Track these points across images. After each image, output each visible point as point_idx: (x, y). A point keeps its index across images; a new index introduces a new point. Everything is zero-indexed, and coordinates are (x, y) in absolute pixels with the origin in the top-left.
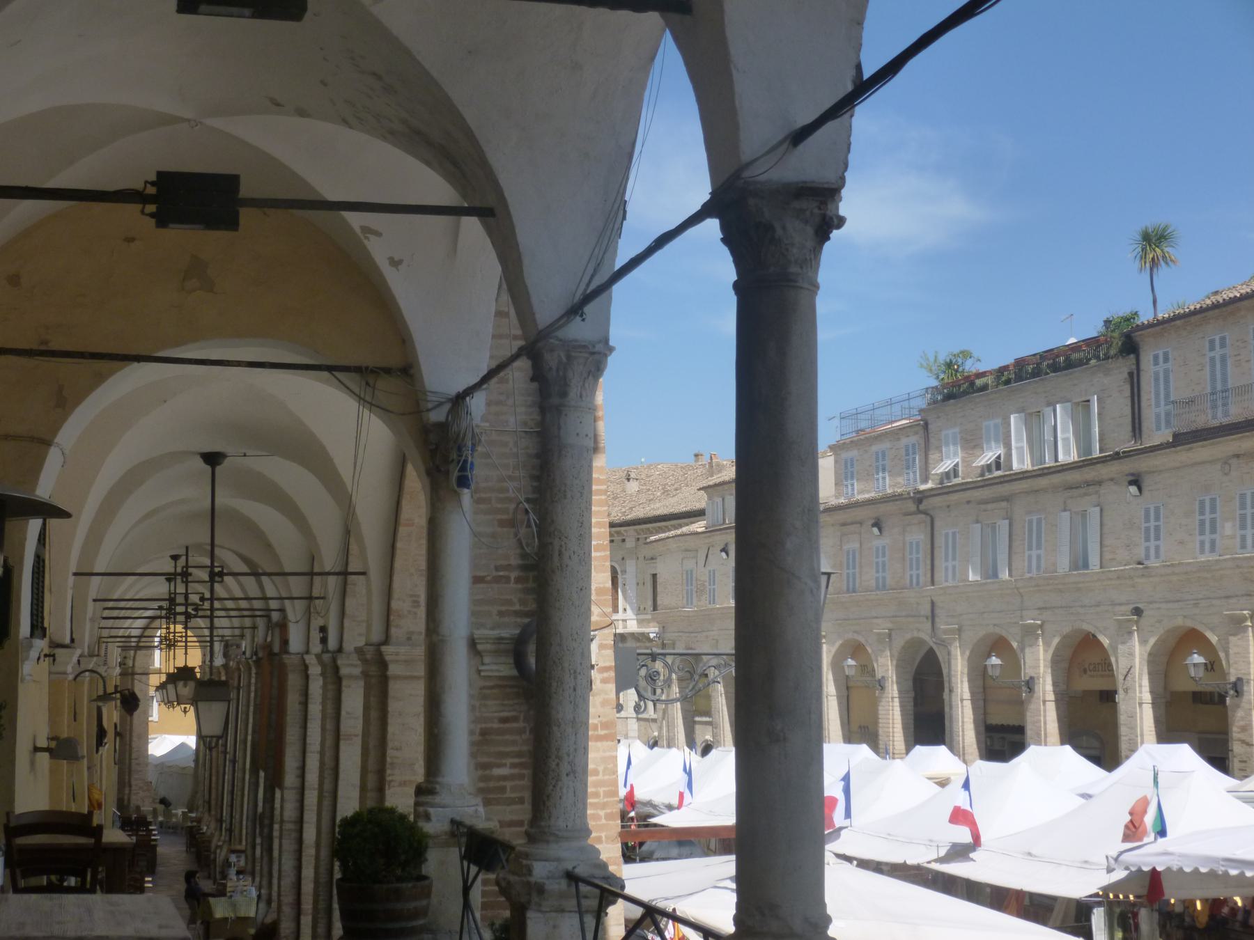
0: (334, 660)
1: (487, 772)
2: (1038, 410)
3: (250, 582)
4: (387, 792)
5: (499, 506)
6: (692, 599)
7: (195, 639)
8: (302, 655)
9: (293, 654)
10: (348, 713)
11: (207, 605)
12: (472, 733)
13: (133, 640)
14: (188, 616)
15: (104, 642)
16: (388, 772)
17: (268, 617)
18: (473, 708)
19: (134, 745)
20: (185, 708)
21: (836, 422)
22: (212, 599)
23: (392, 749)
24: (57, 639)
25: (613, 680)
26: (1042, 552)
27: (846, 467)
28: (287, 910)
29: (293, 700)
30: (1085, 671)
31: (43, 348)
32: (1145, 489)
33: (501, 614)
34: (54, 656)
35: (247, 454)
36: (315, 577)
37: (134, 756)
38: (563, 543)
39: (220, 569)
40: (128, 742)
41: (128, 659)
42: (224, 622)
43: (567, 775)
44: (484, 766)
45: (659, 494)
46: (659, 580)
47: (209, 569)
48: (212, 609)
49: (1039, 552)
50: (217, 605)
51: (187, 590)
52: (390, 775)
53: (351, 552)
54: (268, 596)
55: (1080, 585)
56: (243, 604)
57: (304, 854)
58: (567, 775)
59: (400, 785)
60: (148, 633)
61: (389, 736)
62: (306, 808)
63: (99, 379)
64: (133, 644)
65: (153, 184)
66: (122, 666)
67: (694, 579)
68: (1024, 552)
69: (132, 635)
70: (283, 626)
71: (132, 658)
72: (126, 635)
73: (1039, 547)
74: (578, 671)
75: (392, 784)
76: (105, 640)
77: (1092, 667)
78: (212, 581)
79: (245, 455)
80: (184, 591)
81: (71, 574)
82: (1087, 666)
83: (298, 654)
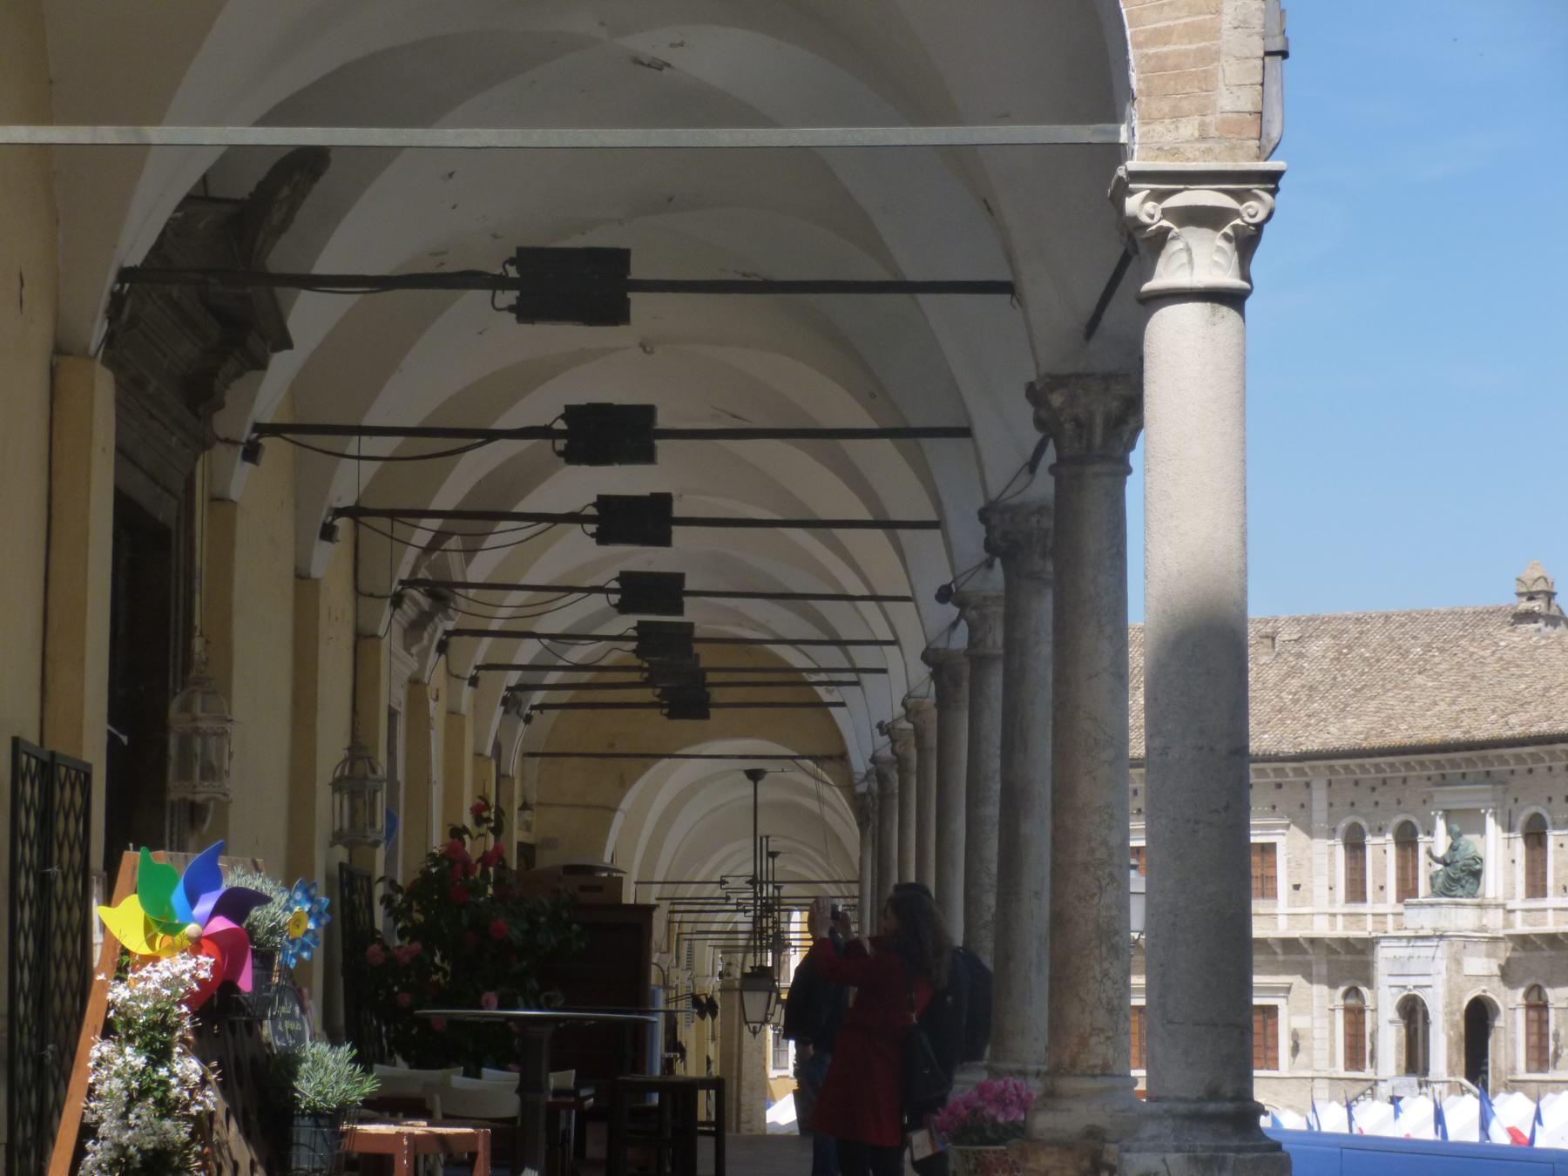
13: (741, 936)
15: (686, 940)
19: (744, 1100)
20: (754, 1028)
31: (611, 751)
37: (744, 1117)
40: (734, 1096)
41: (733, 967)
63: (646, 768)
64: (741, 943)
66: (726, 978)
71: (739, 965)
72: (728, 930)
76: (688, 936)
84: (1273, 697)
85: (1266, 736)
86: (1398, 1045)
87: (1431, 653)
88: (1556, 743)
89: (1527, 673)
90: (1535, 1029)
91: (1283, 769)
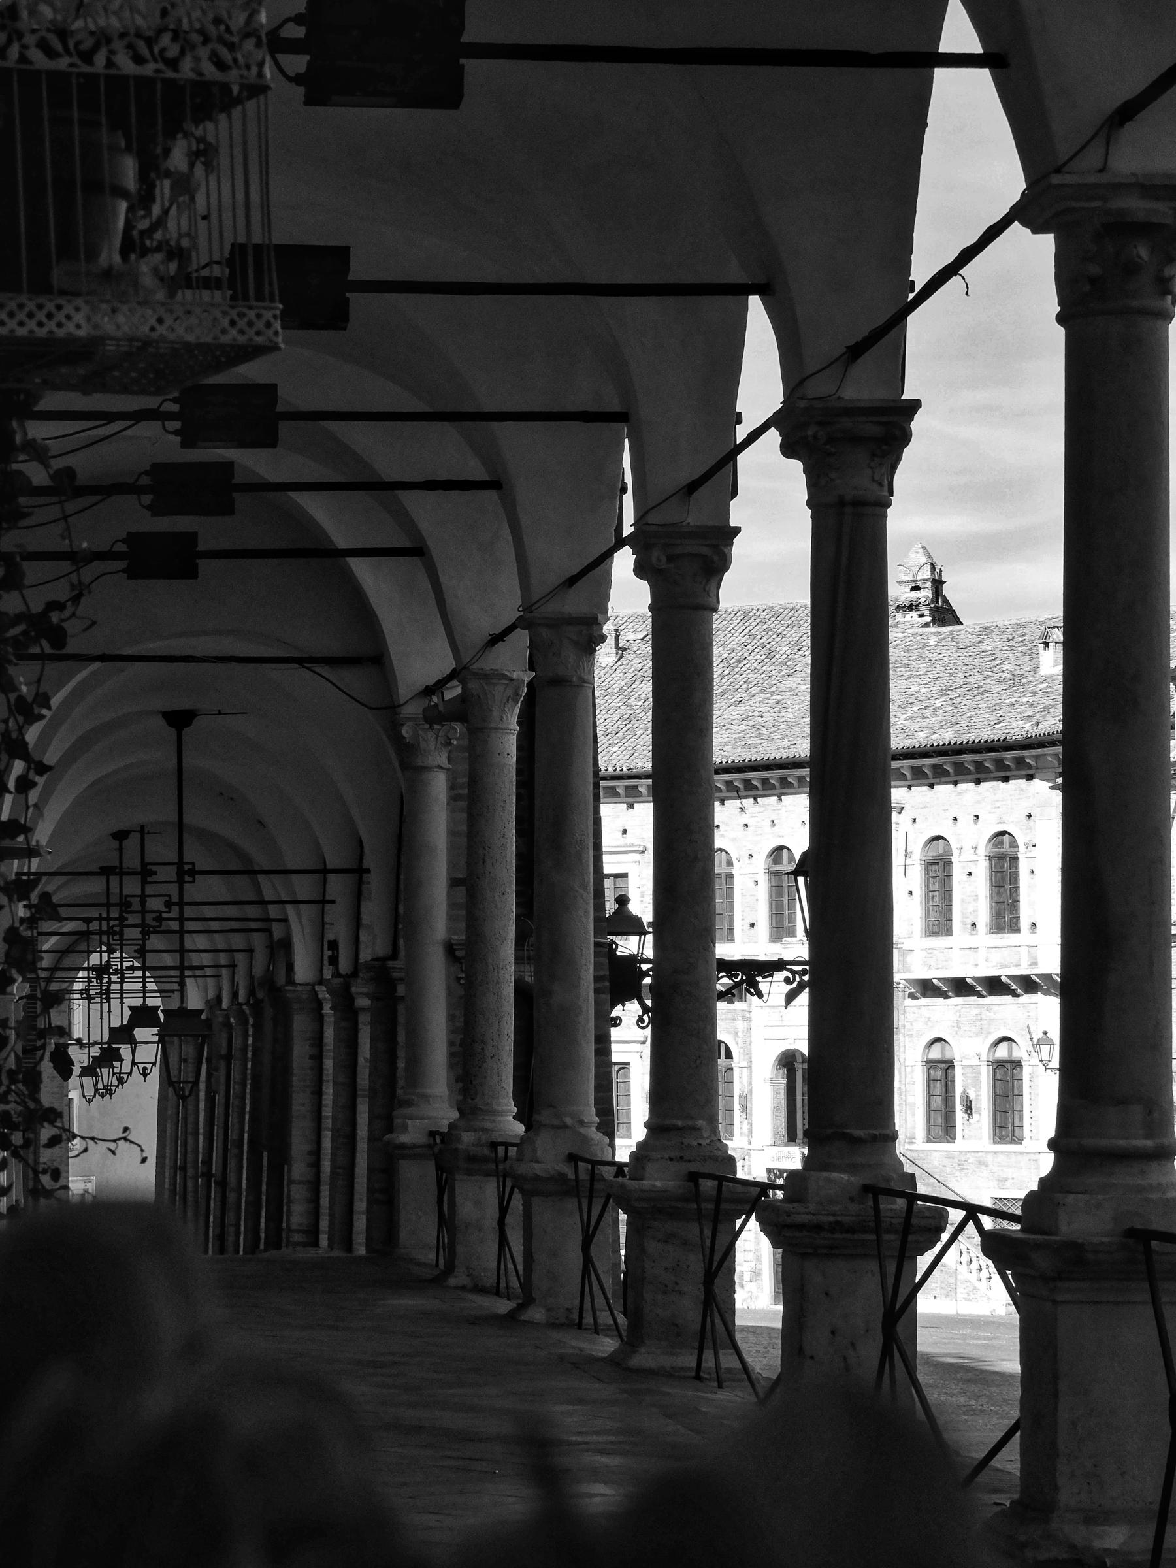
0: (346, 987)
7: (152, 980)
8: (313, 986)
9: (300, 985)
11: (175, 911)
14: (146, 931)
17: (268, 931)
20: (145, 1069)
22: (181, 904)
29: (300, 1051)
35: (222, 712)
39: (190, 866)
42: (201, 942)
43: (491, 1057)
48: (181, 919)
50: (189, 912)
51: (143, 890)
54: (267, 899)
58: (491, 1057)
60: (69, 961)
70: (286, 945)
74: (501, 967)
78: (181, 882)
79: (220, 713)
80: (139, 893)
83: (308, 984)
84: (619, 705)
85: (615, 749)
86: (776, 1108)
87: (801, 653)
88: (965, 753)
89: (917, 673)
90: (938, 1089)
91: (636, 787)
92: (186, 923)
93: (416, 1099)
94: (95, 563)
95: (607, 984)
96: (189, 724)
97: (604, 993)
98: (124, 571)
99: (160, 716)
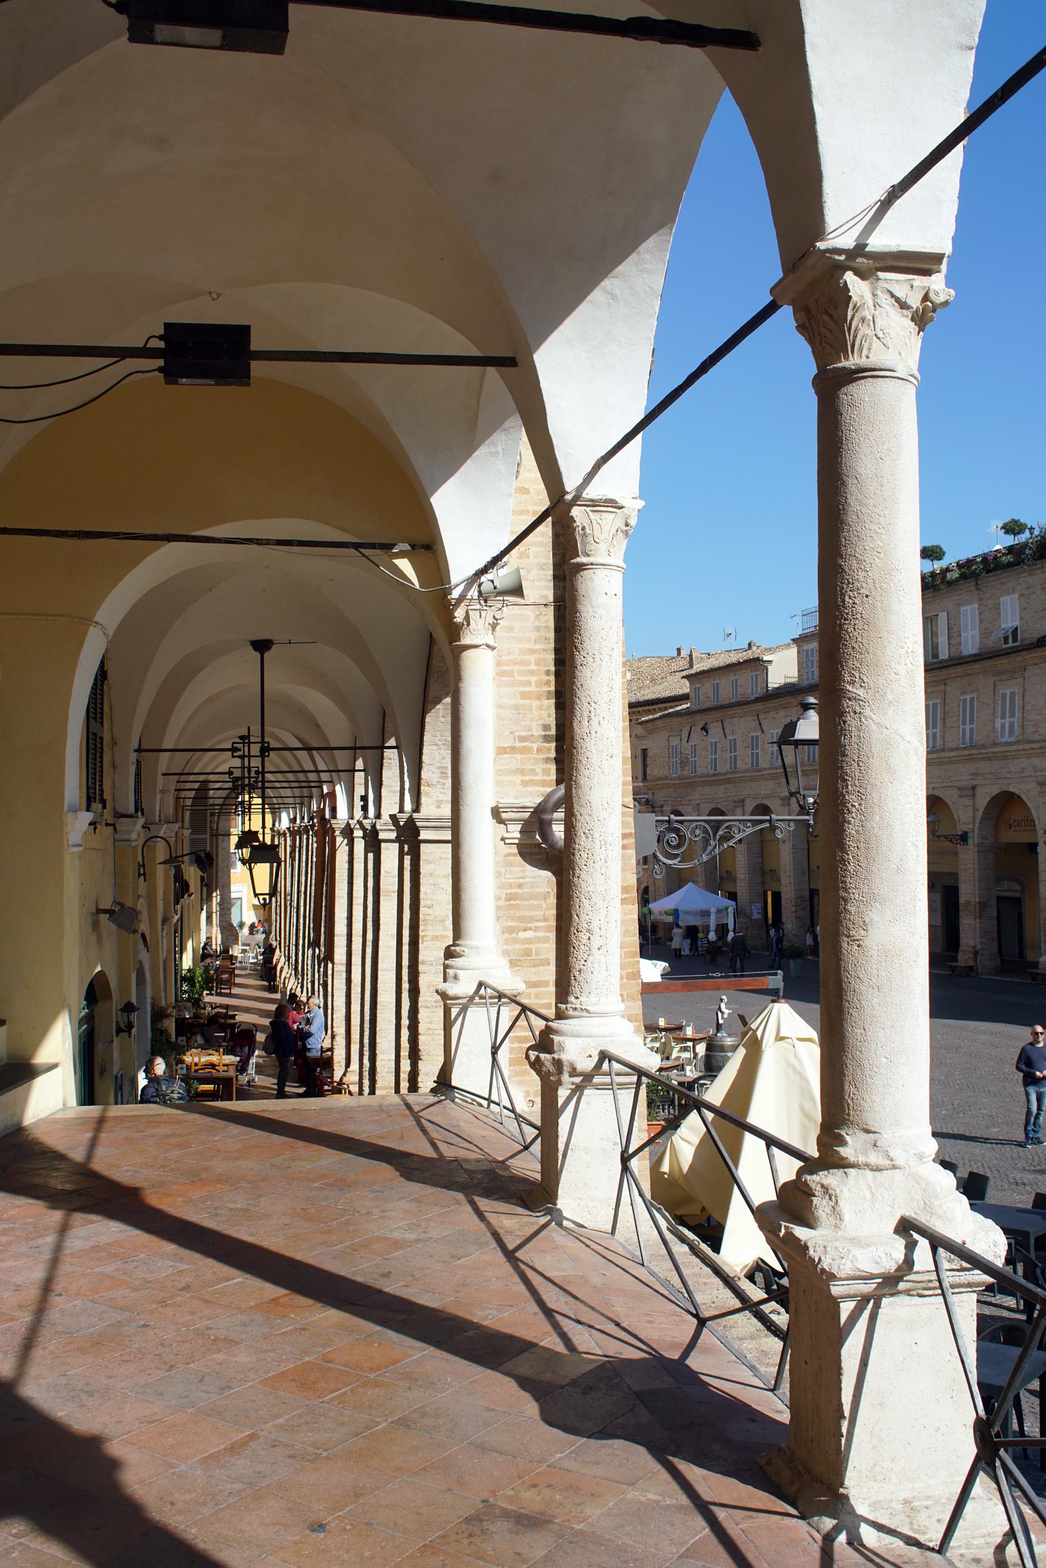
1: (514, 935)
2: (935, 614)
3: (303, 755)
4: (420, 946)
5: (521, 678)
6: (676, 769)
10: (387, 872)
12: (498, 898)
13: (217, 807)
16: (421, 928)
18: (498, 875)
21: (799, 619)
23: (424, 906)
24: (121, 809)
25: (633, 846)
26: (974, 726)
27: (807, 657)
28: (340, 1041)
30: (1010, 827)
32: (710, 732)
33: (524, 783)
34: (114, 825)
36: (357, 751)
38: (592, 708)
43: (599, 949)
44: (510, 930)
45: (648, 682)
46: (650, 754)
47: (260, 745)
49: (972, 726)
52: (422, 931)
53: (386, 729)
55: (1007, 754)
56: (301, 777)
57: (352, 992)
59: (433, 939)
61: (422, 896)
62: (353, 952)
64: (217, 811)
65: (160, 338)
67: (678, 753)
68: (959, 727)
69: (216, 803)
73: (972, 721)
74: (609, 842)
75: (425, 938)
77: (1016, 823)
79: (290, 643)
81: (132, 751)
82: (1012, 822)
92: (266, 775)
93: (466, 950)
94: (128, 360)
95: (633, 840)
96: (269, 648)
97: (629, 849)
98: (160, 370)
99: (249, 643)
